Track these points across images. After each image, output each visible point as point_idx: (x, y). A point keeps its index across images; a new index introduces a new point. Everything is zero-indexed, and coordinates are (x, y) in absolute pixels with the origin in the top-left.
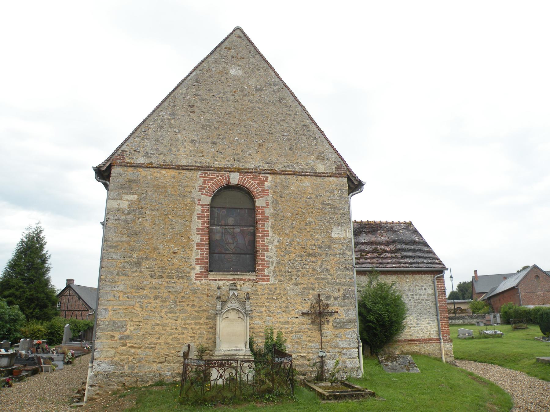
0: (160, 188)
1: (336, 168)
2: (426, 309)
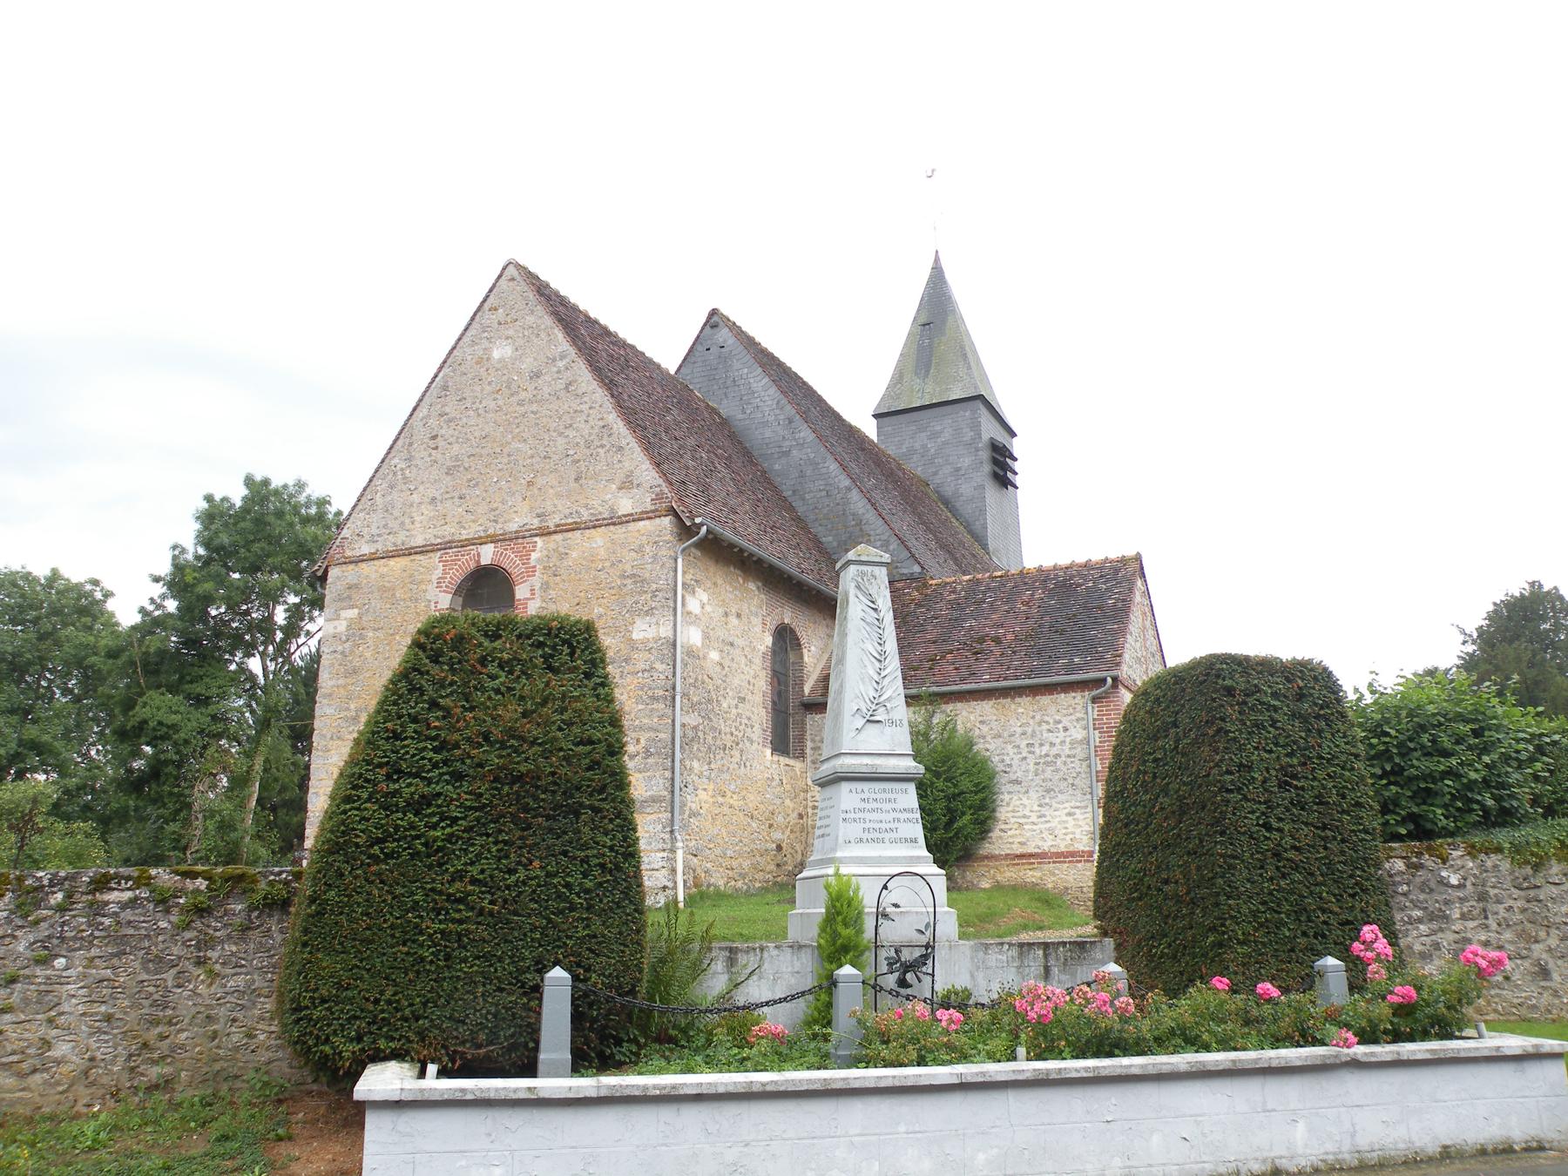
0: (386, 591)
1: (652, 500)
2: (1065, 779)
